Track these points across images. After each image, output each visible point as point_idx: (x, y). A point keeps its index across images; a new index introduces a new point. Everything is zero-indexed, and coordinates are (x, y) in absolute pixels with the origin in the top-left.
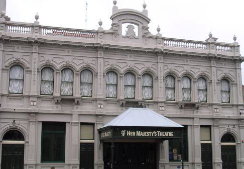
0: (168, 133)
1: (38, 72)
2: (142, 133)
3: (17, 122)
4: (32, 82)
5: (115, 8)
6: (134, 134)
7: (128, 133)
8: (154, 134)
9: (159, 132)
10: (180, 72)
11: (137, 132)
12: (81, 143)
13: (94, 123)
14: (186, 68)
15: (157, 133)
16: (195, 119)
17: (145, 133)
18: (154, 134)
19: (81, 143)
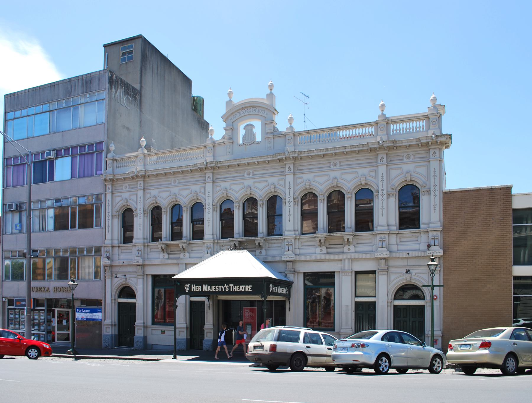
0: (244, 286)
1: (144, 214)
2: (209, 287)
3: (413, 271)
4: (432, 208)
5: (229, 103)
6: (200, 289)
7: (192, 288)
8: (225, 288)
9: (231, 285)
10: (108, 204)
11: (204, 285)
12: (356, 303)
13: (375, 271)
14: (248, 182)
15: (229, 288)
16: (180, 265)
17: (213, 287)
18: (225, 288)
19: (356, 303)
